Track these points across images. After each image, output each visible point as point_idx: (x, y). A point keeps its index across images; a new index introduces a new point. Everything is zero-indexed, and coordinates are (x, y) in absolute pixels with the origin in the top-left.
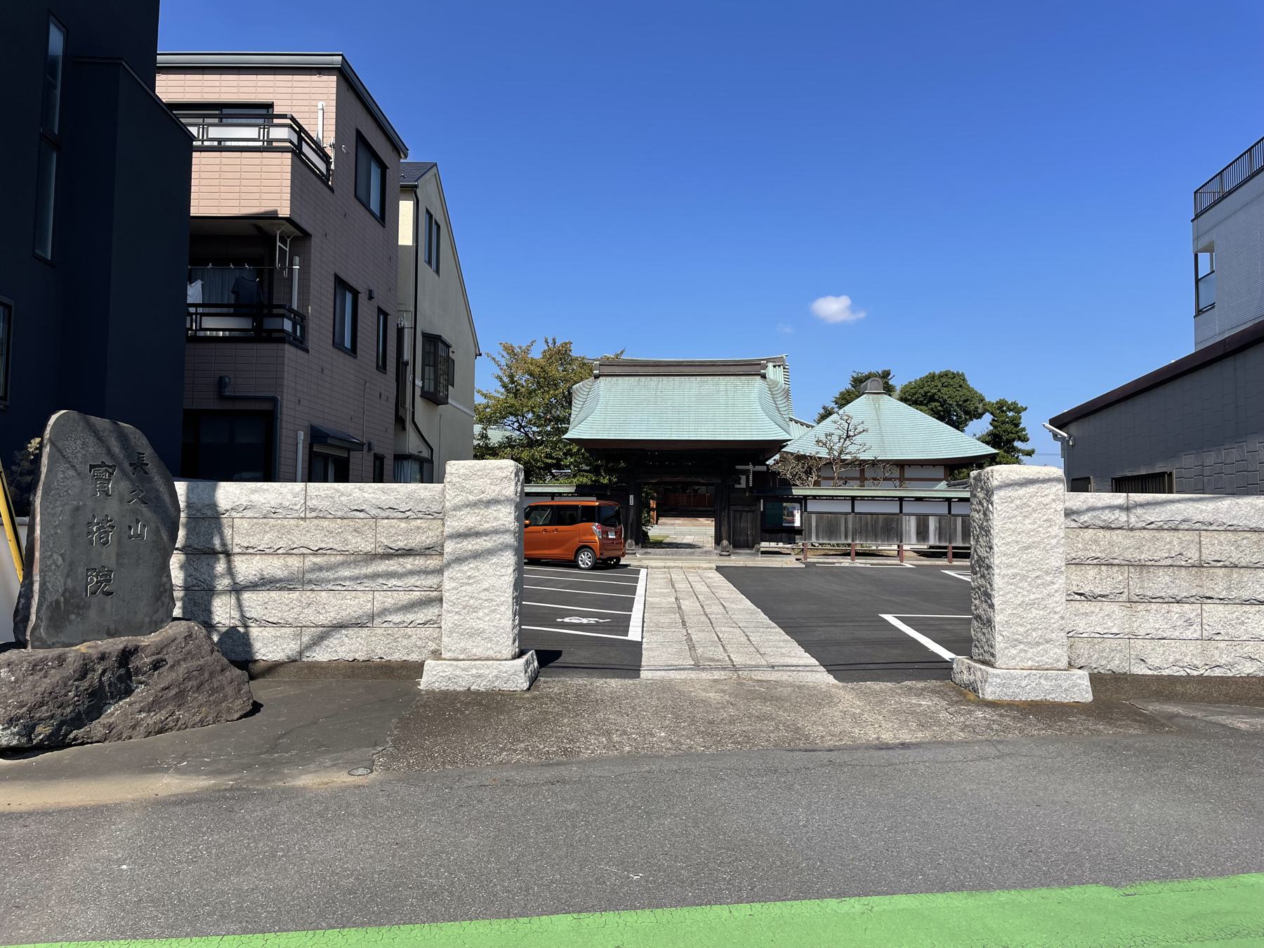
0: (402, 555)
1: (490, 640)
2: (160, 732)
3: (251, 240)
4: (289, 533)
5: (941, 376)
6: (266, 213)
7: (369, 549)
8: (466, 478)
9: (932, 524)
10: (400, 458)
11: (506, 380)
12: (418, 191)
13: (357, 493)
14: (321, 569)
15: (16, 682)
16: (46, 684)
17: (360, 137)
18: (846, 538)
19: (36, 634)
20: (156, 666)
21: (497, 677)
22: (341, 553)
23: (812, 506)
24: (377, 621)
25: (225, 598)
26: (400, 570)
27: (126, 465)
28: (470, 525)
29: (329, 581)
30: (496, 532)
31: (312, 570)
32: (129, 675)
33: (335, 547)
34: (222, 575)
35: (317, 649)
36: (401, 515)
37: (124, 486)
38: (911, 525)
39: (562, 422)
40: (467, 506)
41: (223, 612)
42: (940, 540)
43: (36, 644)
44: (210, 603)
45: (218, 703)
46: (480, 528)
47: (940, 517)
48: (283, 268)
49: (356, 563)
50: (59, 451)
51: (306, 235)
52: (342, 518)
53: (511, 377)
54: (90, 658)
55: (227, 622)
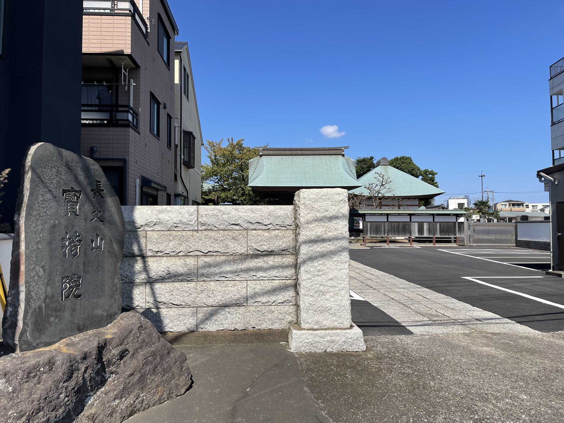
0: (266, 255)
1: (334, 314)
2: (131, 415)
3: (110, 67)
4: (187, 241)
5: (401, 159)
6: (116, 51)
7: (243, 251)
8: (315, 201)
9: (426, 226)
10: (177, 195)
11: (213, 157)
12: (181, 54)
13: (233, 213)
14: (210, 266)
15: (14, 392)
16: (40, 391)
17: (159, 15)
18: (384, 234)
19: (24, 339)
20: (122, 356)
21: (345, 342)
22: (224, 254)
23: (368, 219)
24: (250, 302)
25: (142, 288)
26: (265, 265)
27: (89, 189)
28: (319, 234)
29: (216, 275)
30: (336, 239)
31: (204, 267)
32: (103, 368)
33: (220, 250)
34: (140, 272)
35: (209, 322)
36: (264, 227)
37: (88, 208)
38: (415, 227)
39: (245, 180)
40: (316, 220)
41: (141, 298)
42: (429, 234)
43: (24, 347)
44: (131, 292)
45: (168, 382)
46: (325, 236)
47: (429, 223)
48: (125, 85)
49: (234, 261)
50: (39, 177)
51: (137, 67)
52: (224, 230)
53: (215, 156)
54: (75, 359)
55: (143, 305)
